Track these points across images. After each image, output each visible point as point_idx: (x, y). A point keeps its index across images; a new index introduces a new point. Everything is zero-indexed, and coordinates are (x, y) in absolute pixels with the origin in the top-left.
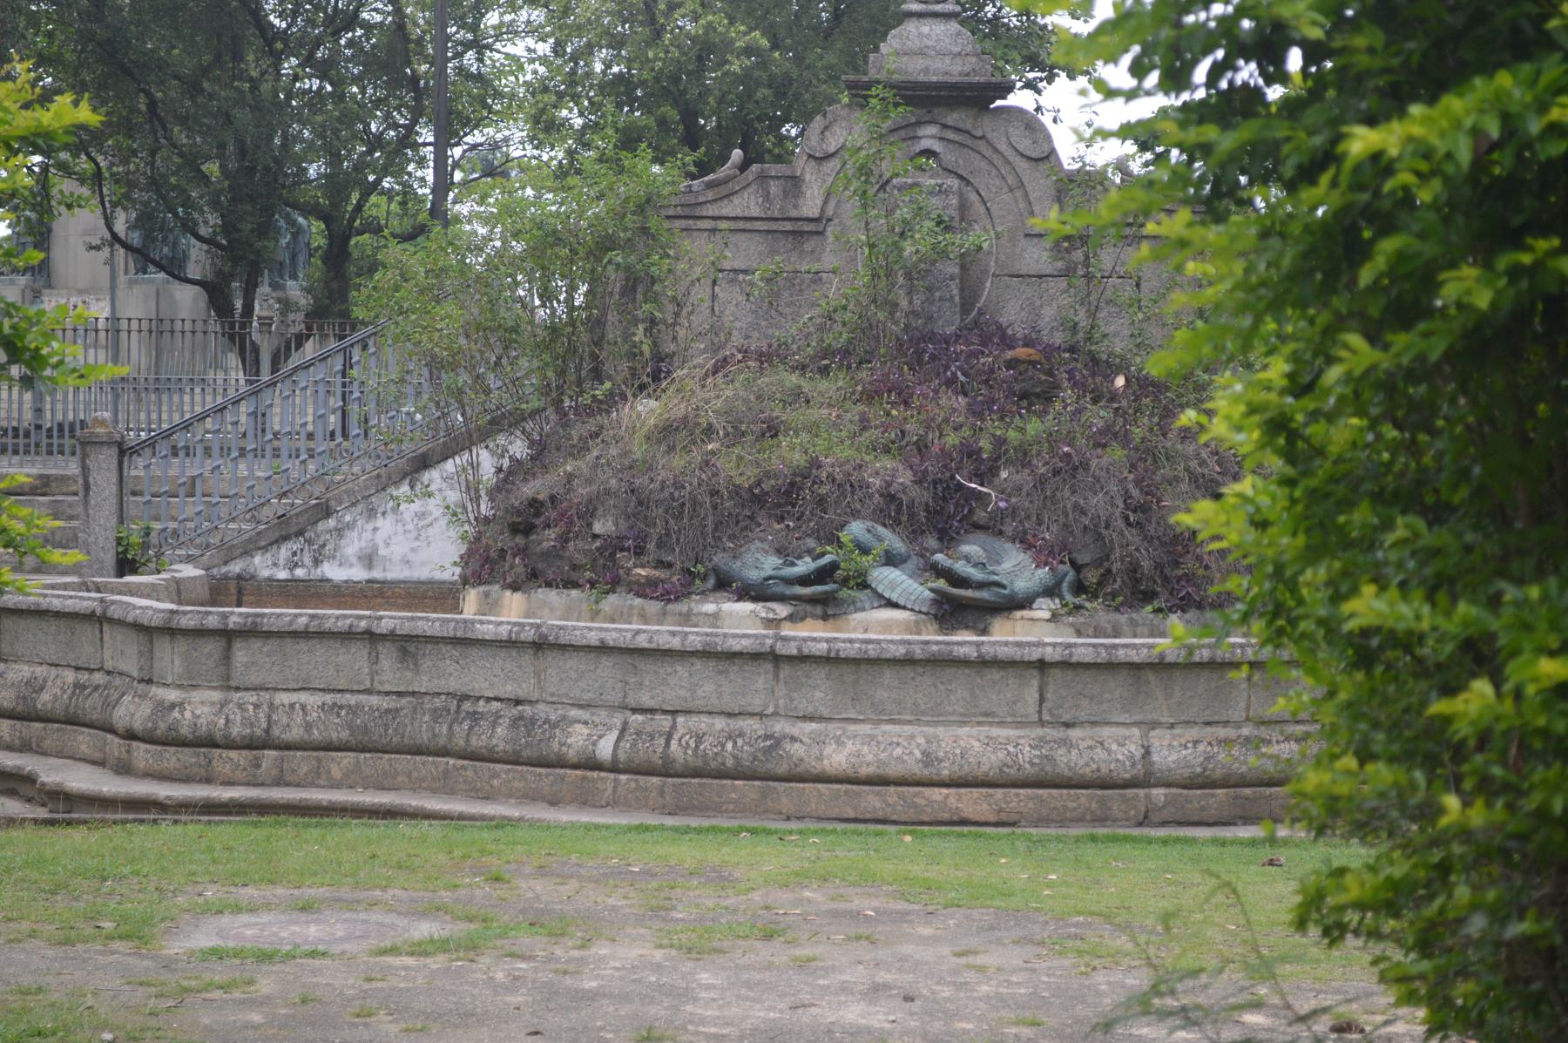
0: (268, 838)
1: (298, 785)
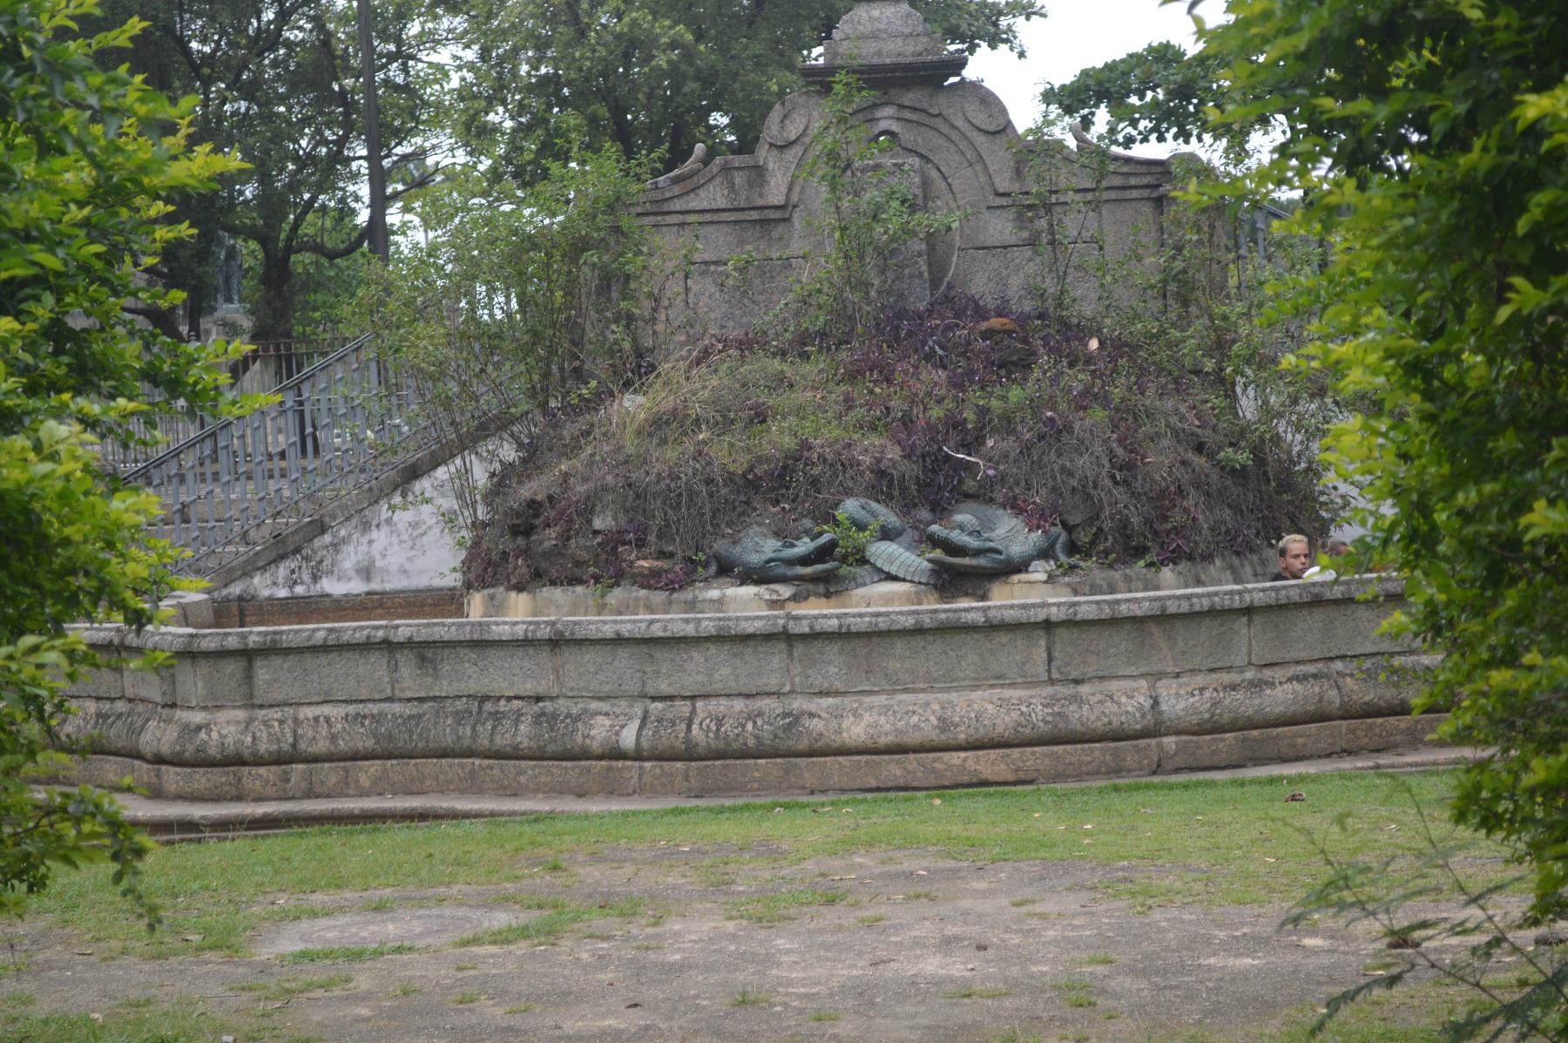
0: (319, 848)
1: (328, 796)
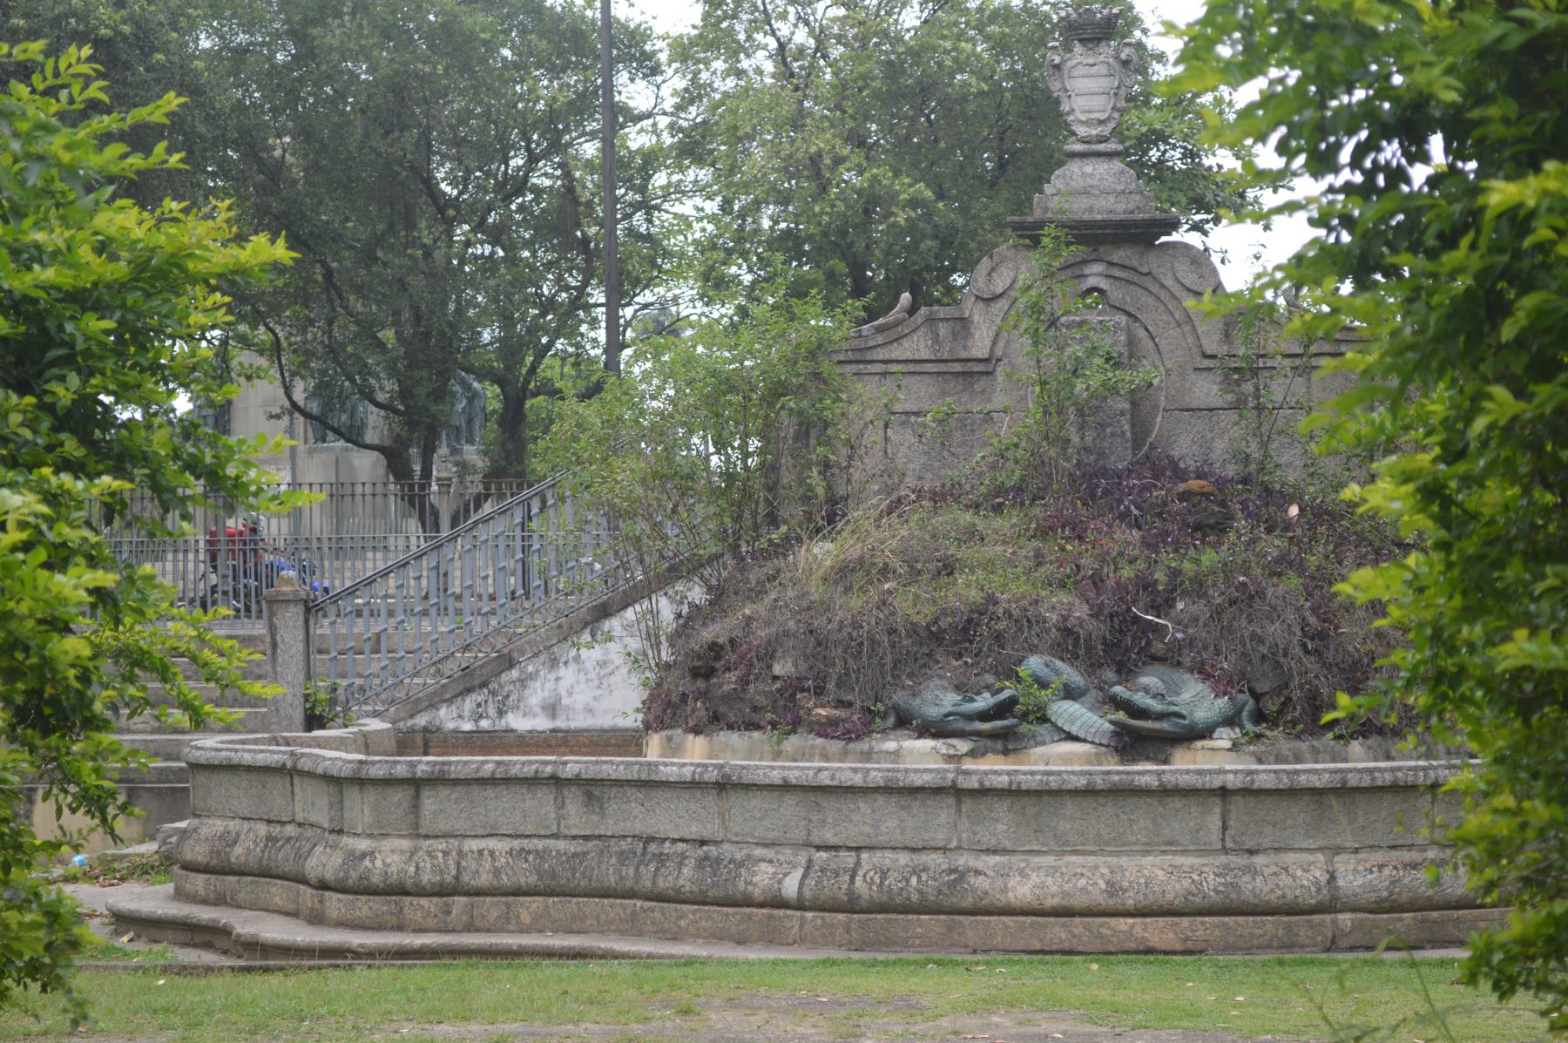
1: (488, 931)
